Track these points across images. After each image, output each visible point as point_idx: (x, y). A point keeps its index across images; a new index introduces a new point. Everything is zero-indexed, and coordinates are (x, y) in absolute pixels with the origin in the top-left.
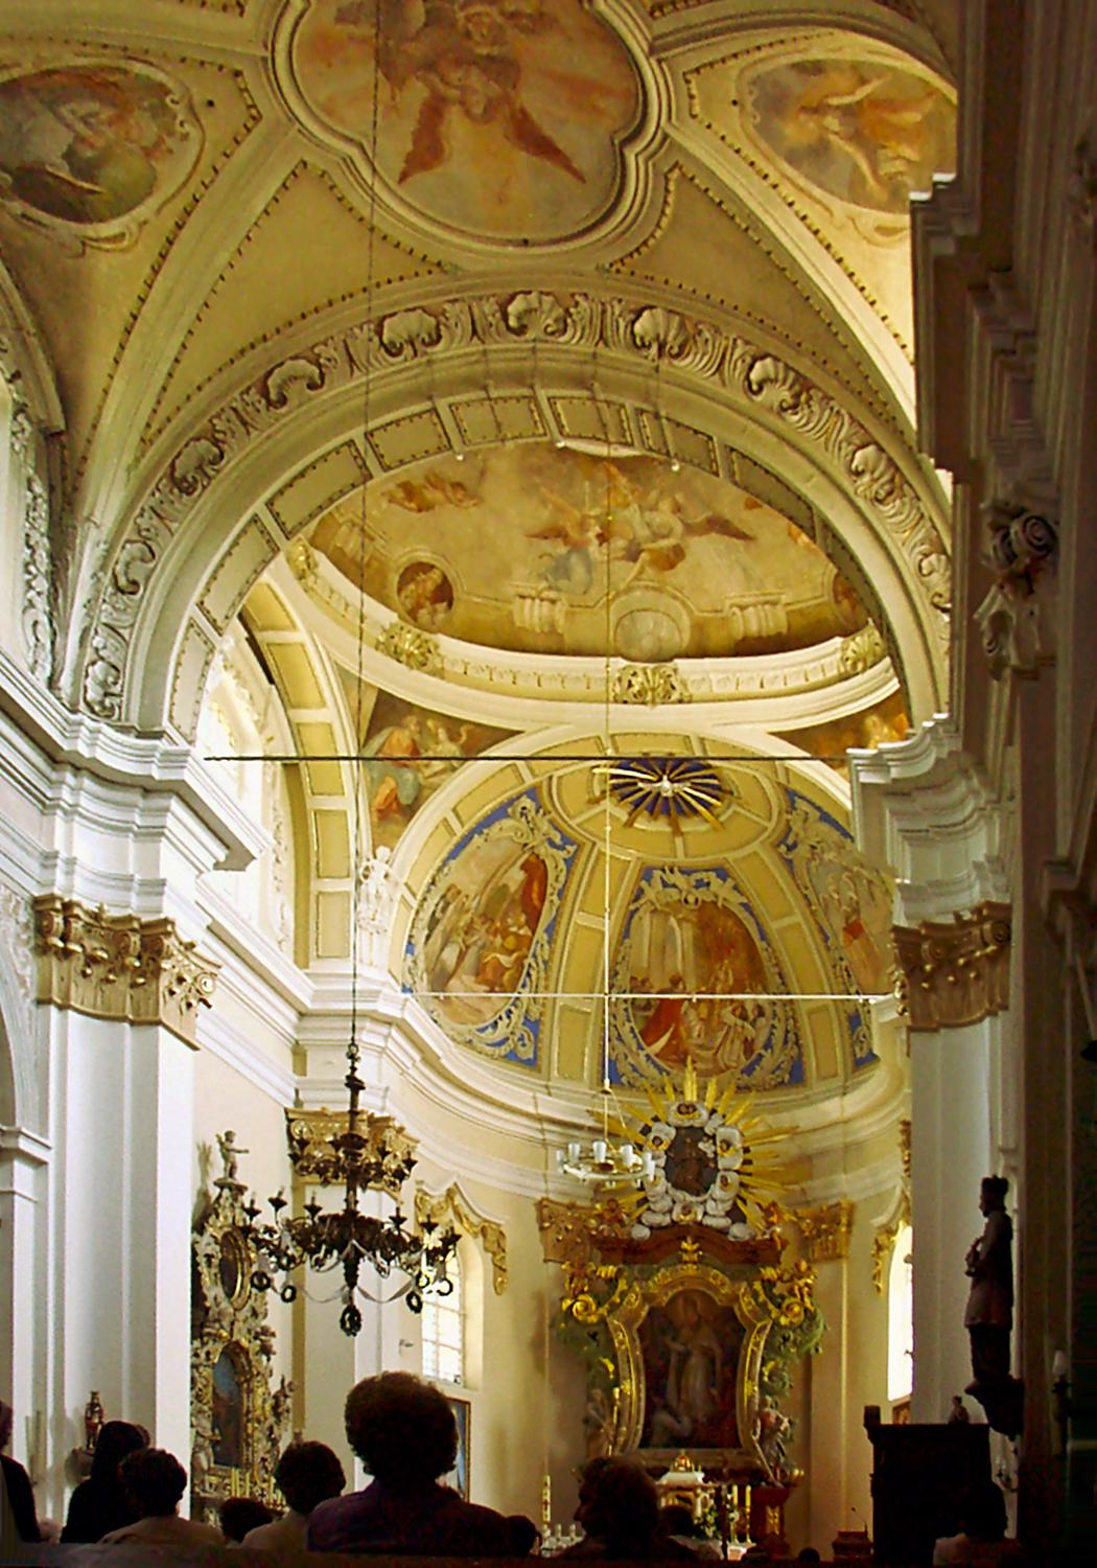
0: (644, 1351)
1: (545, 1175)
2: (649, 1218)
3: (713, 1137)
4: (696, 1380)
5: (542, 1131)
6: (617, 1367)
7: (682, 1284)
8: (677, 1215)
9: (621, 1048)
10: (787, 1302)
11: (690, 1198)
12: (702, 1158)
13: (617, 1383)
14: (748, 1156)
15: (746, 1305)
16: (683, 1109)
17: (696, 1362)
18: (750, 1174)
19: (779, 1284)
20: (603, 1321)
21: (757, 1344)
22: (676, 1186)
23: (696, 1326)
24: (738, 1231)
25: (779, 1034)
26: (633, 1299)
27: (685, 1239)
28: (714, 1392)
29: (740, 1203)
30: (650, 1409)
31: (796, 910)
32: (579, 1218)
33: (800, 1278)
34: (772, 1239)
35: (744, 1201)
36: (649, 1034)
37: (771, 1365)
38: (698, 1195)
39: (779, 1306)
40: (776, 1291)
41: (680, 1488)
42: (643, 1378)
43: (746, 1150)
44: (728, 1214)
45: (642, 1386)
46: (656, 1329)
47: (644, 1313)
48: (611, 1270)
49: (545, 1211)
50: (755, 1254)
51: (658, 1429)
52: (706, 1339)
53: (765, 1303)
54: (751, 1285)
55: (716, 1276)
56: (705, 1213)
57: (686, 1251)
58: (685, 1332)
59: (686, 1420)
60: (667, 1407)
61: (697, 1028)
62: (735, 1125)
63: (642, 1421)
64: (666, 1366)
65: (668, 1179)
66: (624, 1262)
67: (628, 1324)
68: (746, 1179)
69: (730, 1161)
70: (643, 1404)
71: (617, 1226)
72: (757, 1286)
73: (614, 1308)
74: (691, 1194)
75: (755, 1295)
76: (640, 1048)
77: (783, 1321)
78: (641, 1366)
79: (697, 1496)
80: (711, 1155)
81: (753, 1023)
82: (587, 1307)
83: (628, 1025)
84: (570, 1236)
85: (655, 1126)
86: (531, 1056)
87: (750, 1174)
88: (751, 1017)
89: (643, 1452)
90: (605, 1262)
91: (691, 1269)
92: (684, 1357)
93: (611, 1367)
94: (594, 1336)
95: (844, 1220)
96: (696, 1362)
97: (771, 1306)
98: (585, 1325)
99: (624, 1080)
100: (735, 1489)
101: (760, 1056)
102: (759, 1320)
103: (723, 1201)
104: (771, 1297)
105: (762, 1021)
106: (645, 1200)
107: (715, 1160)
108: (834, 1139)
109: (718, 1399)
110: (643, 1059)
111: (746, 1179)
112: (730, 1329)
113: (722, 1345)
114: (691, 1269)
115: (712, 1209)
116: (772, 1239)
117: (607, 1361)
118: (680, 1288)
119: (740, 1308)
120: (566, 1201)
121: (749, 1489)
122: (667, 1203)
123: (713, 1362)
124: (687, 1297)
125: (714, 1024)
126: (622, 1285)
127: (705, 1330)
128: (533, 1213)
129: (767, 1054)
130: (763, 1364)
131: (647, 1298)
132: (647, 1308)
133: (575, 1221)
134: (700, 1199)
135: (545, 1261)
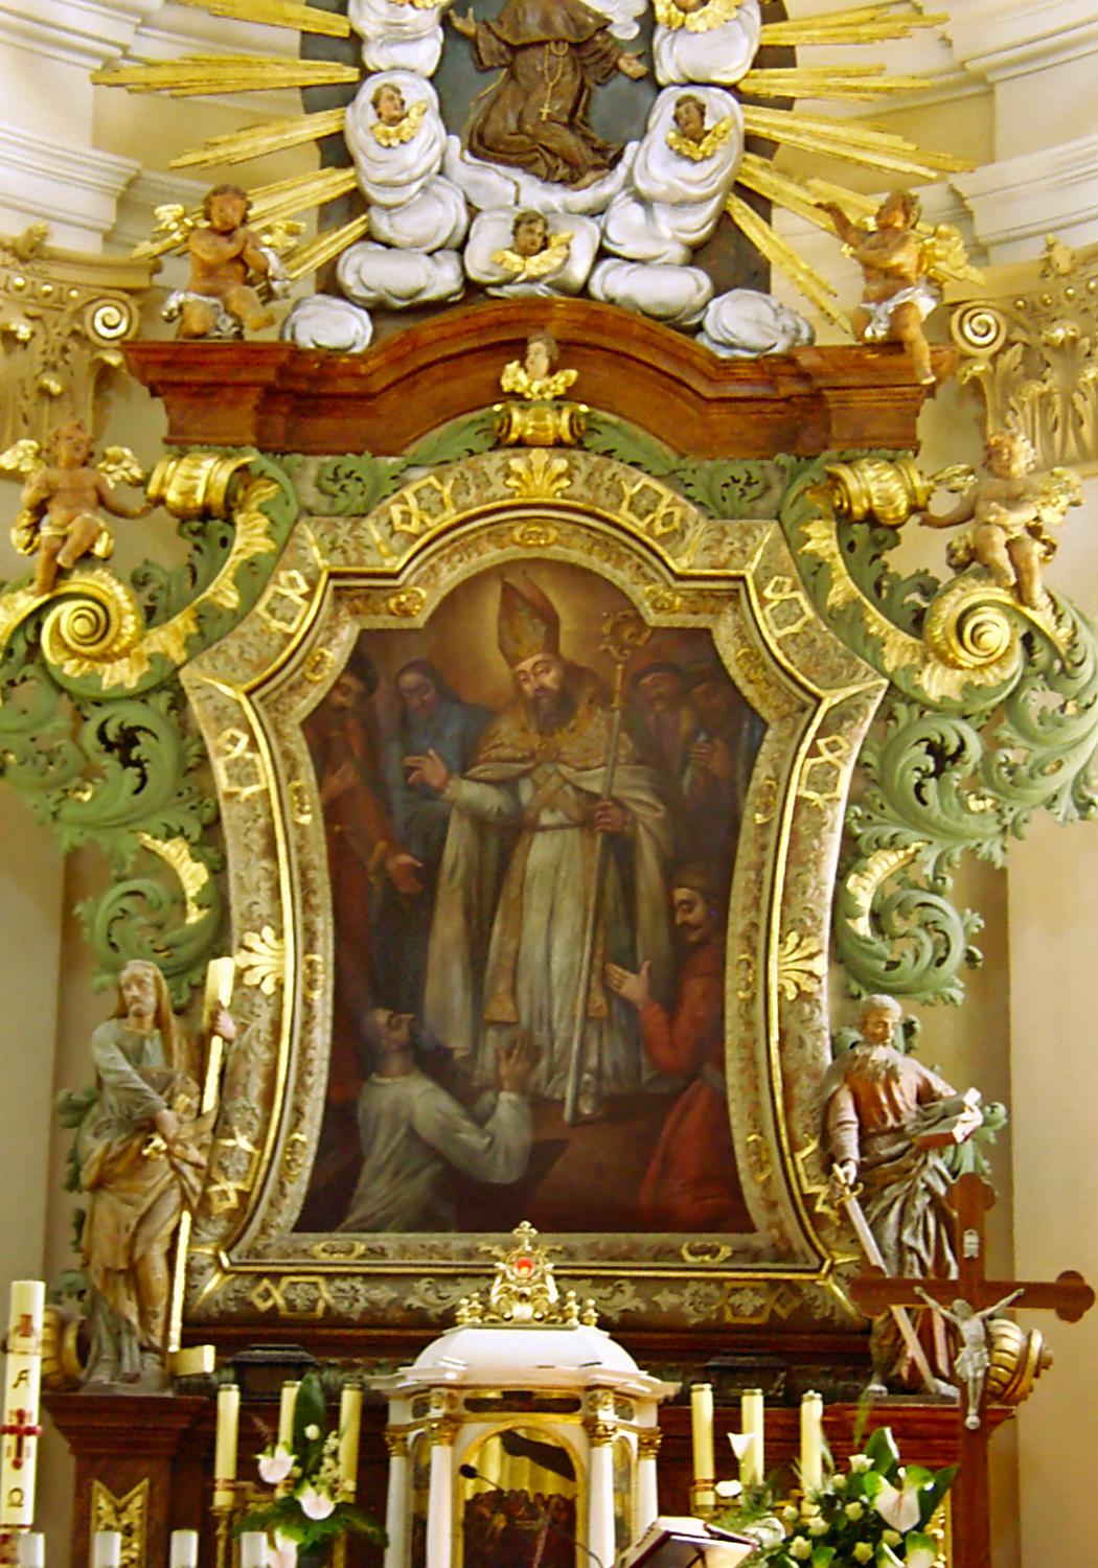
0: (332, 812)
2: (371, 272)
4: (552, 936)
6: (218, 870)
7: (496, 535)
10: (948, 609)
11: (538, 195)
13: (218, 940)
15: (777, 617)
17: (552, 858)
18: (786, 104)
19: (911, 530)
20: (168, 687)
21: (823, 780)
22: (483, 147)
23: (556, 710)
24: (739, 323)
26: (295, 604)
27: (517, 349)
28: (633, 986)
29: (745, 218)
30: (354, 1059)
32: (59, 303)
33: (1013, 501)
35: (762, 205)
37: (882, 865)
38: (571, 181)
39: (917, 623)
40: (901, 561)
41: (521, 1400)
42: (324, 924)
44: (696, 254)
45: (324, 957)
46: (379, 720)
47: (336, 656)
48: (201, 476)
50: (802, 413)
51: (381, 1148)
52: (597, 759)
53: (854, 608)
54: (793, 539)
55: (647, 500)
56: (602, 254)
58: (510, 735)
59: (507, 1106)
60: (434, 1063)
63: (315, 1108)
64: (430, 870)
65: (449, 118)
67: (269, 692)
68: (767, 122)
70: (322, 1036)
71: (244, 299)
72: (822, 539)
73: (210, 630)
74: (548, 178)
75: (814, 576)
77: (936, 683)
78: (321, 878)
79: (594, 1433)
82: (102, 627)
87: (786, 104)
88: (350, 74)
89: (317, 1244)
90: (179, 443)
91: (540, 475)
92: (505, 836)
93: (193, 876)
94: (124, 744)
96: (552, 858)
97: (877, 622)
98: (82, 703)
100: (753, 1406)
102: (834, 680)
103: (681, 204)
104: (878, 588)
106: (355, 202)
109: (654, 1017)
111: (767, 122)
112: (699, 717)
113: (664, 791)
114: (540, 475)
115: (633, 238)
116: (895, 345)
117: (175, 852)
118: (491, 555)
119: (746, 633)
121: (812, 1409)
122: (446, 216)
123: (620, 850)
124: (519, 591)
126: (250, 537)
127: (595, 728)
130: (853, 854)
131: (352, 588)
132: (348, 633)
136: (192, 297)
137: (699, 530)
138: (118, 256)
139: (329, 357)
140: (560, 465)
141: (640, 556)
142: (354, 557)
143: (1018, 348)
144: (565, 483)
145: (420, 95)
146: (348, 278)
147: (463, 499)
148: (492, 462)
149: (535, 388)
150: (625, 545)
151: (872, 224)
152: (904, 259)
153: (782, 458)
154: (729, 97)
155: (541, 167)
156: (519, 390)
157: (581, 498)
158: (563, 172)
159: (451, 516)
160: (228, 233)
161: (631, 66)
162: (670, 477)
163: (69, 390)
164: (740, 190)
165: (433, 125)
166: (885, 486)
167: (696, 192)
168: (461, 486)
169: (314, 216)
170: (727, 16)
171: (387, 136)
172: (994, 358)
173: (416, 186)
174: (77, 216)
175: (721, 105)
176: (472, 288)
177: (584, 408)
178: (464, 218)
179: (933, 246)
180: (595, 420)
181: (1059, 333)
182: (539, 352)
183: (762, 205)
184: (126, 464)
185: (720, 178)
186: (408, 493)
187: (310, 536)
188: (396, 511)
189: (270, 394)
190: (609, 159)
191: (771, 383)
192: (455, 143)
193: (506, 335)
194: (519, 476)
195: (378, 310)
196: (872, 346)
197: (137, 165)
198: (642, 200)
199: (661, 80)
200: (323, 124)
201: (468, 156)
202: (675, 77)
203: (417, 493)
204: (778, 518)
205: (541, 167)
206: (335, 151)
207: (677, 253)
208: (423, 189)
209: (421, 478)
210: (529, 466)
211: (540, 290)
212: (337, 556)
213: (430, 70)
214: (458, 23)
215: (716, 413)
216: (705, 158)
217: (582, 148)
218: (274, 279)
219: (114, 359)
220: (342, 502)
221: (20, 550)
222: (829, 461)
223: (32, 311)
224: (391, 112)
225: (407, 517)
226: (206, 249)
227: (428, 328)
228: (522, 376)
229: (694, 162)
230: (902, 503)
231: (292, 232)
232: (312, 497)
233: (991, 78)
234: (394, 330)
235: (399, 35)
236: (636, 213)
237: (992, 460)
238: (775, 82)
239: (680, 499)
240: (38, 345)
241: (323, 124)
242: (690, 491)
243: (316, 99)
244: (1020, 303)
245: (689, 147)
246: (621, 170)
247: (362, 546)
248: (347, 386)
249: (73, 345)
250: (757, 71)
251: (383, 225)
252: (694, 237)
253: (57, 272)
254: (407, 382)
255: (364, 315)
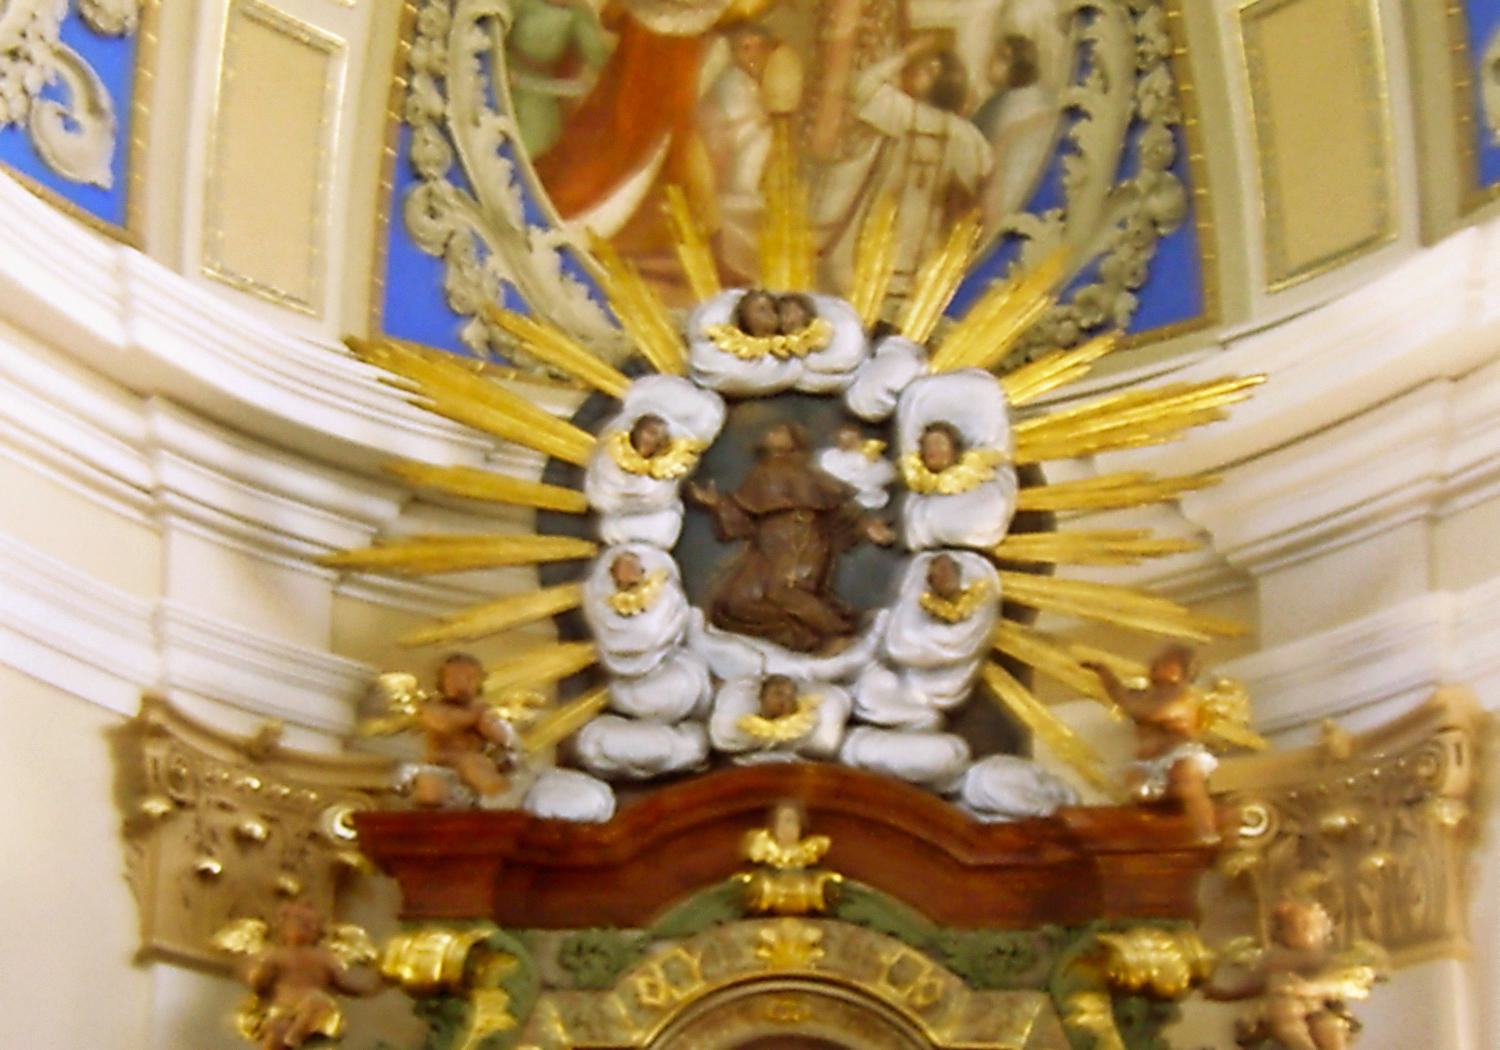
1: (157, 619)
3: (884, 428)
5: (148, 448)
7: (744, 1007)
8: (734, 720)
9: (458, 219)
12: (833, 513)
14: (1034, 499)
16: (761, 316)
18: (1040, 569)
22: (726, 617)
24: (996, 788)
25: (1097, 137)
27: (761, 818)
31: (763, 728)
33: (1310, 970)
34: (1170, 804)
35: (1018, 670)
36: (569, 166)
43: (1028, 476)
44: (952, 720)
48: (434, 952)
49: (154, 752)
55: (903, 970)
56: (852, 722)
57: (763, 867)
61: (755, 151)
62: (951, 394)
65: (689, 587)
66: (505, 922)
68: (1022, 587)
69: (965, 510)
71: (478, 768)
76: (534, 217)
80: (871, 499)
81: (985, 120)
83: (493, 125)
84: (255, 862)
85: (637, 397)
86: (103, 177)
87: (1040, 569)
90: (414, 917)
91: (790, 946)
95: (1456, 777)
99: (471, 333)
101: (1013, 238)
103: (936, 669)
105: (1026, 105)
106: (592, 676)
107: (892, 515)
108: (1389, 463)
110: (544, 261)
111: (1022, 587)
115: (883, 704)
116: (1170, 804)
120: (241, 727)
122: (683, 687)
125: (826, 131)
126: (487, 1014)
128: (98, 768)
129: (1040, 230)
133: (275, 811)
134: (828, 666)
135: (147, 956)
136: (427, 768)
137: (961, 1001)
138: (353, 758)
139: (566, 829)
140: (813, 934)
141: (901, 1030)
142: (598, 1031)
143: (1291, 841)
144: (820, 953)
145: (659, 566)
146: (588, 749)
147: (711, 970)
148: (740, 931)
149: (786, 859)
150: (885, 1020)
151: (1142, 683)
152: (1178, 711)
153: (1048, 928)
154: (985, 562)
155: (787, 636)
156: (770, 860)
157: (835, 969)
158: (811, 640)
159: (698, 987)
160: (458, 701)
161: (877, 533)
162: (930, 949)
163: (303, 891)
164: (996, 656)
165: (673, 595)
166: (1164, 956)
167: (951, 655)
168: (709, 957)
169: (554, 689)
170: (983, 476)
171: (626, 603)
172: (1265, 850)
173: (659, 656)
174: (312, 719)
175: (977, 573)
176: (716, 757)
177: (837, 878)
178: (708, 690)
179: (1213, 701)
180: (850, 891)
181: (1340, 820)
182: (788, 818)
183: (1018, 670)
184: (360, 944)
185: (975, 645)
186: (655, 966)
187: (554, 1013)
188: (641, 983)
189: (508, 865)
190: (853, 626)
191: (1032, 850)
192: (698, 615)
193: (753, 803)
194: (770, 947)
195: (619, 781)
196: (1149, 805)
197: (370, 667)
198: (894, 666)
199: (912, 544)
200: (556, 599)
201: (711, 629)
202: (926, 541)
203: (665, 967)
204: (1047, 989)
205: (787, 636)
206: (571, 626)
207: (930, 718)
208: (664, 660)
209: (665, 950)
210: (782, 939)
211: (788, 757)
212: (582, 1031)
213: (671, 540)
214: (699, 495)
215: (976, 883)
216: (962, 619)
217: (826, 616)
218: (511, 749)
219: (352, 859)
220: (585, 977)
221: (247, 1035)
222: (1101, 930)
223: (268, 812)
224: (627, 578)
225: (653, 988)
226: (440, 719)
227: (672, 797)
228: (772, 847)
229: (947, 622)
230: (1183, 975)
231: (529, 705)
232: (553, 974)
233: (1254, 570)
234: (634, 800)
235: (634, 507)
236: (886, 680)
237: (1283, 930)
238: (1032, 547)
239: (942, 970)
240: (276, 844)
241: (556, 599)
242: (954, 962)
243: (552, 573)
244: (1294, 794)
245: (944, 609)
246: (872, 639)
247: (606, 1020)
248: (588, 857)
249: (311, 847)
250: (1015, 537)
251: (625, 697)
252: (945, 702)
253: (293, 773)
254: (648, 853)
255: (607, 788)
